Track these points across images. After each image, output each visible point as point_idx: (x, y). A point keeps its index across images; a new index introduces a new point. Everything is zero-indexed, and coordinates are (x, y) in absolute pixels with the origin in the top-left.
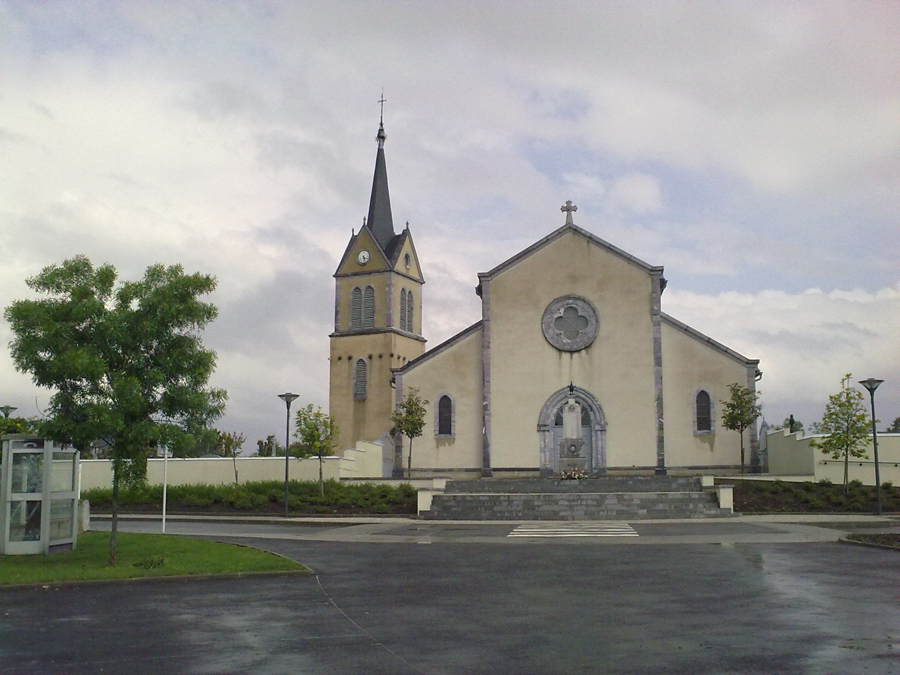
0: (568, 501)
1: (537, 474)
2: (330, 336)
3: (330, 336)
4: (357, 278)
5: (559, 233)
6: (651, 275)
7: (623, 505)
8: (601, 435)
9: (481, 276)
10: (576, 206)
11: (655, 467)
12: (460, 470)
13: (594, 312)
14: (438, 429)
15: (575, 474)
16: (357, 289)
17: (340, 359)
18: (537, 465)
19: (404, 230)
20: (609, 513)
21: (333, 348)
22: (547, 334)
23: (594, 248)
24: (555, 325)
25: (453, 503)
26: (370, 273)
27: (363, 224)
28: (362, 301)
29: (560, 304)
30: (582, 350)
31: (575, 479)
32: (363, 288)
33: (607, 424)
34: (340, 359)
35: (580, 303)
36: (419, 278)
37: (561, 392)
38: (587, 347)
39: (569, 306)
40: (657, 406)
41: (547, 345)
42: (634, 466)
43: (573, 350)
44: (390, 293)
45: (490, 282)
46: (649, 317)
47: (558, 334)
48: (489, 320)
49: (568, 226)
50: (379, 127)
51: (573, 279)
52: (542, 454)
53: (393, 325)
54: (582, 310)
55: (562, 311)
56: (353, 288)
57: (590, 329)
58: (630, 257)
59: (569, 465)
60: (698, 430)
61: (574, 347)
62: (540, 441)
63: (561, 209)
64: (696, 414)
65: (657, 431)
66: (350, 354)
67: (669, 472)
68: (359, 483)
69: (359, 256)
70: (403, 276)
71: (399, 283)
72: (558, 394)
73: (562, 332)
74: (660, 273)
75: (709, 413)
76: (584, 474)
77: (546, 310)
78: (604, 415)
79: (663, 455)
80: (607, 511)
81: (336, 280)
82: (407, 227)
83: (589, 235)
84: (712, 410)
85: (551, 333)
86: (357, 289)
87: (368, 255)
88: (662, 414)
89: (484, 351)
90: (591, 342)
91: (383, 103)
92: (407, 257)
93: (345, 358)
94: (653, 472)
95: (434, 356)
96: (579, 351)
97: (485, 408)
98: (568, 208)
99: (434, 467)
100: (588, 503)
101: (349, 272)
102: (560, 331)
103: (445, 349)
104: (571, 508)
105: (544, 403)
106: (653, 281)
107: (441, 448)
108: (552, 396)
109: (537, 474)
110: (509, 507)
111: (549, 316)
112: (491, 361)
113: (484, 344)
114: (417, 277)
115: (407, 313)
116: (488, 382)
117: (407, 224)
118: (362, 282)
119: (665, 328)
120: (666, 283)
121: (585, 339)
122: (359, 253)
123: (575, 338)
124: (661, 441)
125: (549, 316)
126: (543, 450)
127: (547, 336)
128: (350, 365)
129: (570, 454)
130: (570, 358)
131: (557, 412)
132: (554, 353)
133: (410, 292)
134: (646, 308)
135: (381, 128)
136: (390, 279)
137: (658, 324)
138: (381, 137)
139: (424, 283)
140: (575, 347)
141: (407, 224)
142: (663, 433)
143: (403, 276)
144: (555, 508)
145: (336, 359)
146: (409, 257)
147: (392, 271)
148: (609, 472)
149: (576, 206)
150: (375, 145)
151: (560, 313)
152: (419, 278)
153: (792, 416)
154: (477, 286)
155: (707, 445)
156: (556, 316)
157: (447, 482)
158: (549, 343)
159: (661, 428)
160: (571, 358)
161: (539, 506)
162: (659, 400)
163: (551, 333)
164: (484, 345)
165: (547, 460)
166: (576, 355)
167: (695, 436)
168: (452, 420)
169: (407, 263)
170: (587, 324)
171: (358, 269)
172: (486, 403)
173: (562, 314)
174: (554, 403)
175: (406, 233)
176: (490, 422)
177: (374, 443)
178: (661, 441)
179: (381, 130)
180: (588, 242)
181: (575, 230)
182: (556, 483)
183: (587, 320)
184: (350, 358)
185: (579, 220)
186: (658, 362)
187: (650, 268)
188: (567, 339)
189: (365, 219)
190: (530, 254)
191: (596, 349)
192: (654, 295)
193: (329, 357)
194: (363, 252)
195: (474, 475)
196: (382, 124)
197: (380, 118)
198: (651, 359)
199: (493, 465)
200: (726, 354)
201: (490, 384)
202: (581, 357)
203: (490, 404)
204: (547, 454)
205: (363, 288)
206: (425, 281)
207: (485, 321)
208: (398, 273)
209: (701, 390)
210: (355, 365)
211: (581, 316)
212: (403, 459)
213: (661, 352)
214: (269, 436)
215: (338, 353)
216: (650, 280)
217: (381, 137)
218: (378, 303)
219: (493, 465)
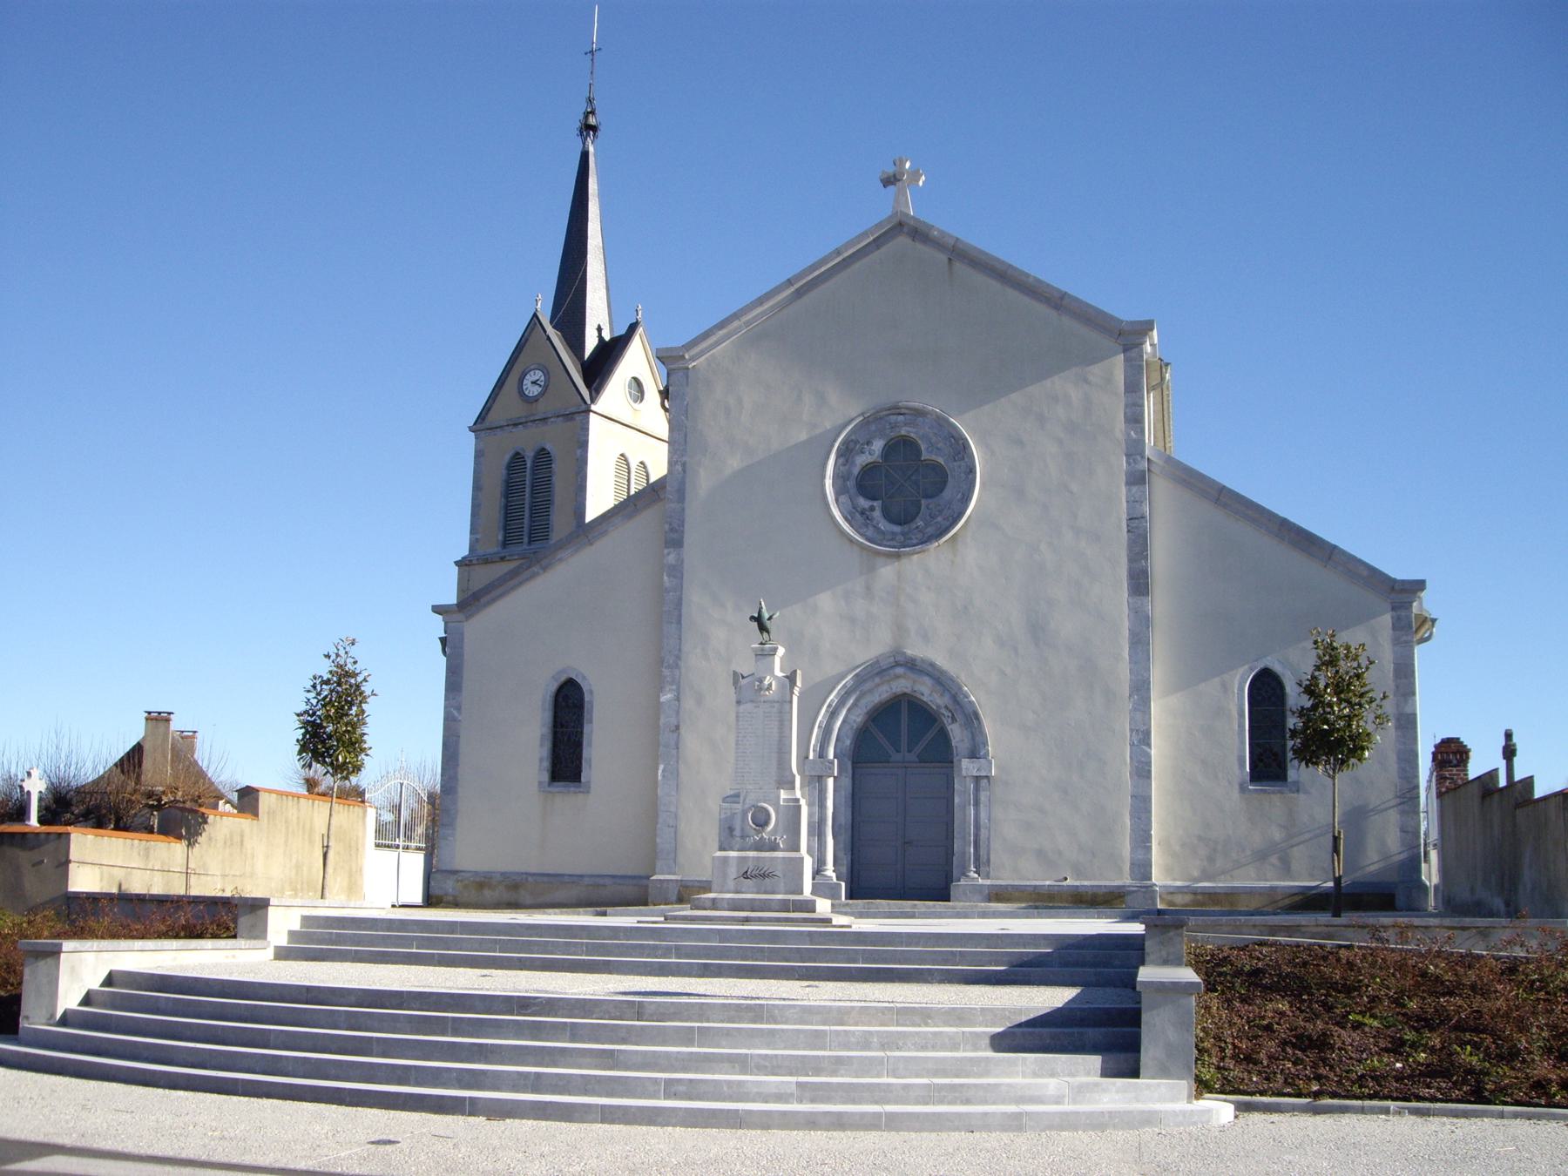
16: (518, 458)
196: (590, 101)
217: (588, 129)
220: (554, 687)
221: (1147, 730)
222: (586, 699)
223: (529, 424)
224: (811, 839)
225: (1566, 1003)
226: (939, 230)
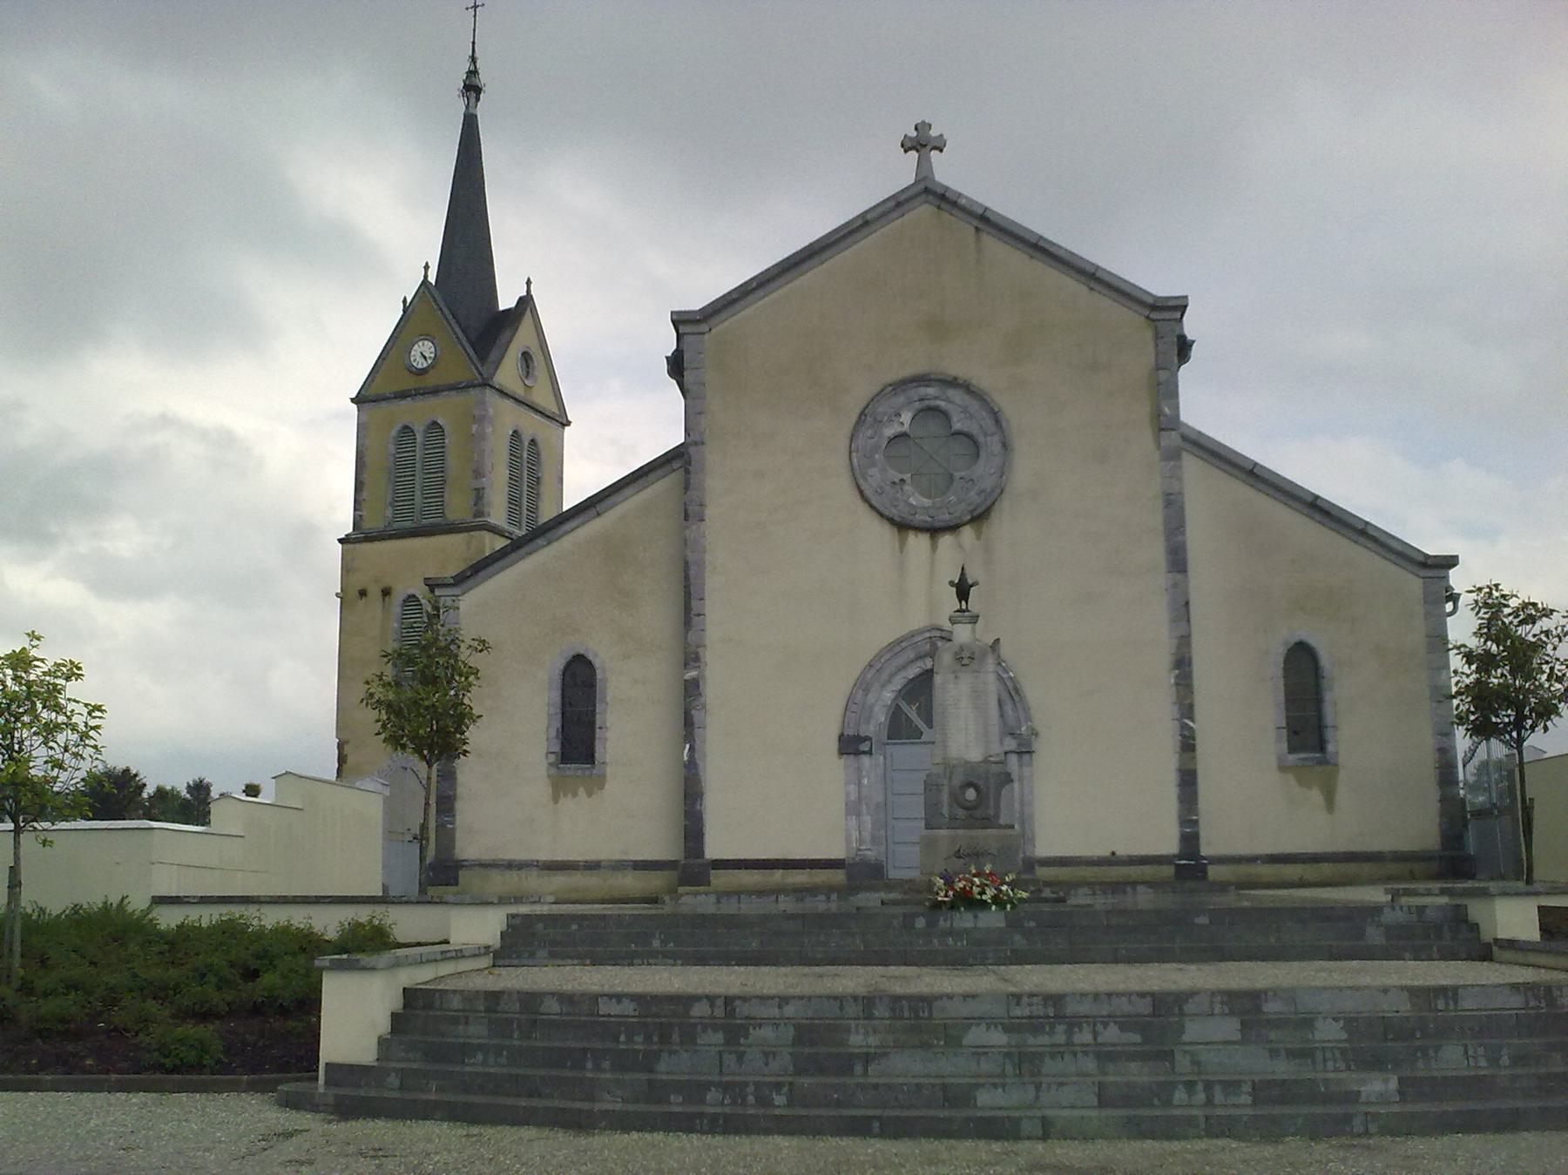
0: (1008, 1029)
1: (838, 876)
2: (340, 541)
3: (340, 541)
4: (406, 404)
5: (898, 204)
6: (1154, 320)
7: (1274, 1053)
8: (1021, 766)
9: (680, 321)
10: (941, 136)
11: (1175, 856)
12: (619, 866)
13: (997, 422)
14: (557, 748)
15: (983, 886)
16: (407, 430)
17: (363, 593)
18: (835, 850)
19: (521, 298)
20: (1219, 1097)
21: (347, 569)
22: (865, 479)
23: (995, 247)
24: (888, 457)
25: (477, 1031)
26: (435, 391)
27: (422, 278)
28: (417, 458)
29: (901, 399)
30: (964, 525)
31: (984, 905)
32: (419, 429)
33: (1037, 735)
34: (363, 593)
35: (956, 395)
36: (557, 412)
37: (904, 644)
38: (979, 518)
39: (927, 402)
40: (1177, 684)
41: (862, 508)
42: (1113, 853)
43: (941, 524)
44: (482, 437)
45: (706, 336)
46: (1147, 435)
47: (897, 480)
48: (703, 443)
49: (922, 186)
50: (467, 66)
51: (938, 329)
52: (853, 822)
53: (489, 515)
54: (962, 415)
55: (906, 417)
56: (398, 427)
57: (984, 470)
58: (1093, 271)
59: (958, 855)
60: (1289, 753)
61: (940, 518)
62: (847, 783)
63: (902, 146)
64: (1283, 706)
65: (1177, 756)
66: (387, 582)
67: (1214, 872)
68: (207, 917)
69: (413, 353)
70: (516, 400)
71: (506, 418)
72: (899, 649)
73: (907, 477)
74: (1178, 315)
75: (1318, 702)
76: (1012, 885)
77: (862, 413)
78: (1026, 710)
79: (1196, 822)
80: (1209, 1086)
81: (358, 411)
82: (528, 291)
83: (980, 211)
84: (1328, 697)
85: (875, 478)
86: (407, 430)
87: (433, 349)
88: (1191, 706)
89: (687, 528)
90: (989, 502)
91: (477, 9)
92: (526, 357)
93: (374, 592)
94: (1168, 871)
95: (549, 544)
96: (953, 528)
97: (692, 691)
98: (921, 143)
99: (544, 856)
100: (1100, 1040)
101: (388, 390)
102: (901, 472)
103: (583, 524)
104: (1024, 1063)
105: (856, 674)
106: (1158, 337)
107: (567, 803)
108: (879, 656)
109: (838, 876)
110: (729, 1060)
111: (869, 433)
112: (708, 557)
113: (690, 508)
114: (552, 408)
115: (525, 488)
116: (699, 615)
117: (529, 282)
118: (417, 413)
119: (1192, 466)
120: (1191, 346)
121: (972, 493)
122: (413, 346)
123: (944, 493)
124: (1188, 781)
125: (869, 433)
126: (853, 809)
127: (864, 486)
128: (385, 610)
129: (961, 813)
130: (929, 546)
131: (894, 699)
132: (886, 533)
133: (533, 442)
134: (1143, 410)
135: (472, 68)
136: (482, 403)
137: (1172, 455)
138: (472, 88)
139: (569, 423)
140: (944, 517)
141: (529, 282)
142: (1194, 758)
143: (516, 400)
144: (950, 1067)
145: (353, 596)
146: (532, 361)
147: (486, 384)
148: (1043, 873)
149: (941, 136)
150: (460, 106)
151: (902, 423)
152: (557, 412)
153: (1561, 716)
154: (669, 354)
155: (1316, 795)
156: (889, 432)
157: (513, 916)
158: (872, 507)
159: (1188, 745)
160: (934, 547)
161: (867, 1059)
162: (1182, 664)
163: (875, 478)
164: (690, 513)
165: (866, 835)
166: (946, 540)
167: (1283, 768)
168: (598, 724)
169: (527, 376)
170: (978, 455)
171: (410, 383)
172: (693, 674)
173: (906, 428)
174: (884, 677)
175: (526, 302)
176: (704, 728)
177: (358, 784)
178: (1188, 781)
179: (473, 73)
180: (977, 229)
181: (943, 197)
182: (920, 923)
183: (975, 443)
184: (386, 593)
185: (947, 171)
186: (1178, 561)
187: (1151, 301)
188: (922, 495)
189: (427, 267)
190: (816, 259)
191: (1002, 526)
192: (1163, 375)
193: (339, 591)
194: (420, 343)
195: (655, 882)
196: (473, 59)
197: (471, 45)
198: (1157, 552)
199: (713, 850)
200: (1361, 539)
201: (704, 603)
202: (960, 546)
203: (703, 677)
204: (867, 819)
205: (419, 429)
206: (570, 419)
207: (691, 445)
208: (503, 393)
209: (1297, 639)
210: (396, 609)
211: (959, 433)
212: (458, 835)
213: (1183, 534)
214: (248, 782)
215: (358, 581)
216: (1149, 334)
217: (472, 88)
218: (452, 461)
219: (713, 850)
220: (560, 664)
221: (1189, 704)
222: (599, 677)
223: (393, 396)
224: (849, 818)
225: (2, 968)
226: (966, 198)
